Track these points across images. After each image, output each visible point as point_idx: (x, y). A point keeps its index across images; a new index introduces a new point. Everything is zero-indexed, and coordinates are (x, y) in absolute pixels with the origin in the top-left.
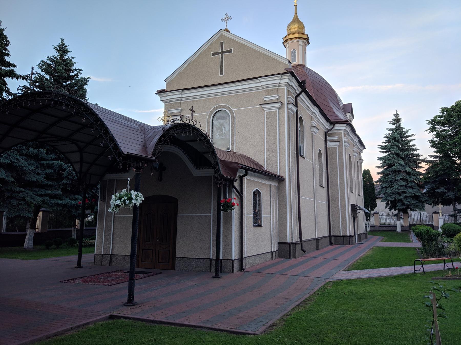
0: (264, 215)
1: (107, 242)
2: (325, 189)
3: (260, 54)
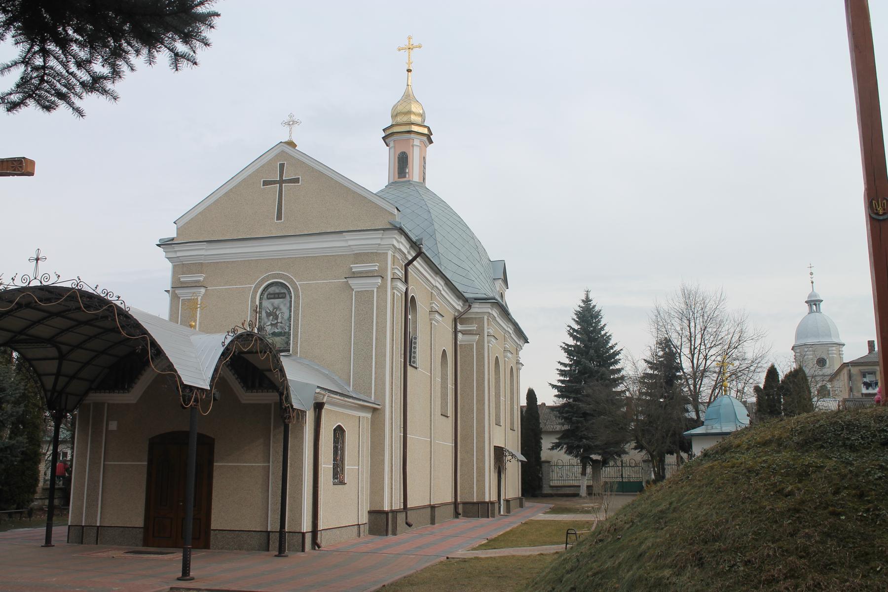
0: (349, 467)
1: (92, 505)
2: (450, 422)
3: (348, 190)
